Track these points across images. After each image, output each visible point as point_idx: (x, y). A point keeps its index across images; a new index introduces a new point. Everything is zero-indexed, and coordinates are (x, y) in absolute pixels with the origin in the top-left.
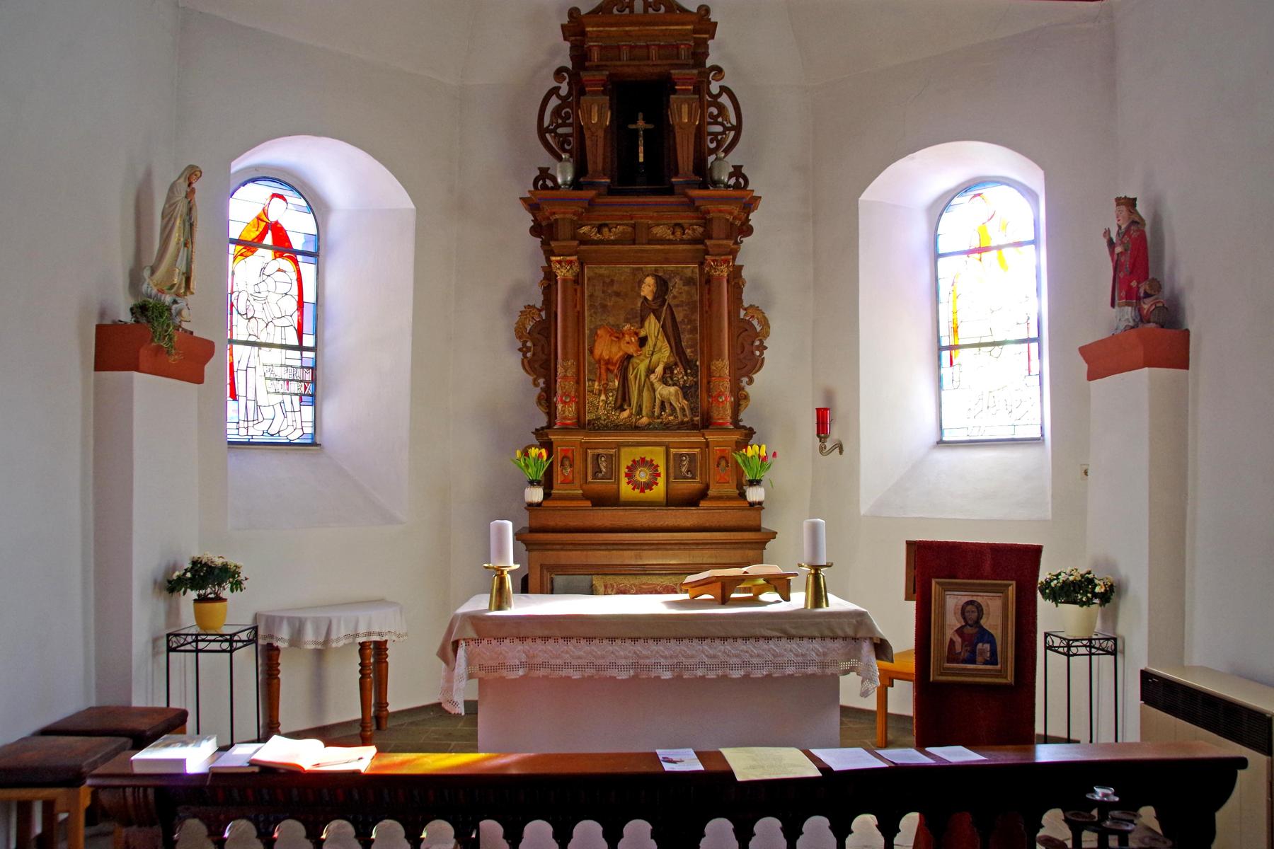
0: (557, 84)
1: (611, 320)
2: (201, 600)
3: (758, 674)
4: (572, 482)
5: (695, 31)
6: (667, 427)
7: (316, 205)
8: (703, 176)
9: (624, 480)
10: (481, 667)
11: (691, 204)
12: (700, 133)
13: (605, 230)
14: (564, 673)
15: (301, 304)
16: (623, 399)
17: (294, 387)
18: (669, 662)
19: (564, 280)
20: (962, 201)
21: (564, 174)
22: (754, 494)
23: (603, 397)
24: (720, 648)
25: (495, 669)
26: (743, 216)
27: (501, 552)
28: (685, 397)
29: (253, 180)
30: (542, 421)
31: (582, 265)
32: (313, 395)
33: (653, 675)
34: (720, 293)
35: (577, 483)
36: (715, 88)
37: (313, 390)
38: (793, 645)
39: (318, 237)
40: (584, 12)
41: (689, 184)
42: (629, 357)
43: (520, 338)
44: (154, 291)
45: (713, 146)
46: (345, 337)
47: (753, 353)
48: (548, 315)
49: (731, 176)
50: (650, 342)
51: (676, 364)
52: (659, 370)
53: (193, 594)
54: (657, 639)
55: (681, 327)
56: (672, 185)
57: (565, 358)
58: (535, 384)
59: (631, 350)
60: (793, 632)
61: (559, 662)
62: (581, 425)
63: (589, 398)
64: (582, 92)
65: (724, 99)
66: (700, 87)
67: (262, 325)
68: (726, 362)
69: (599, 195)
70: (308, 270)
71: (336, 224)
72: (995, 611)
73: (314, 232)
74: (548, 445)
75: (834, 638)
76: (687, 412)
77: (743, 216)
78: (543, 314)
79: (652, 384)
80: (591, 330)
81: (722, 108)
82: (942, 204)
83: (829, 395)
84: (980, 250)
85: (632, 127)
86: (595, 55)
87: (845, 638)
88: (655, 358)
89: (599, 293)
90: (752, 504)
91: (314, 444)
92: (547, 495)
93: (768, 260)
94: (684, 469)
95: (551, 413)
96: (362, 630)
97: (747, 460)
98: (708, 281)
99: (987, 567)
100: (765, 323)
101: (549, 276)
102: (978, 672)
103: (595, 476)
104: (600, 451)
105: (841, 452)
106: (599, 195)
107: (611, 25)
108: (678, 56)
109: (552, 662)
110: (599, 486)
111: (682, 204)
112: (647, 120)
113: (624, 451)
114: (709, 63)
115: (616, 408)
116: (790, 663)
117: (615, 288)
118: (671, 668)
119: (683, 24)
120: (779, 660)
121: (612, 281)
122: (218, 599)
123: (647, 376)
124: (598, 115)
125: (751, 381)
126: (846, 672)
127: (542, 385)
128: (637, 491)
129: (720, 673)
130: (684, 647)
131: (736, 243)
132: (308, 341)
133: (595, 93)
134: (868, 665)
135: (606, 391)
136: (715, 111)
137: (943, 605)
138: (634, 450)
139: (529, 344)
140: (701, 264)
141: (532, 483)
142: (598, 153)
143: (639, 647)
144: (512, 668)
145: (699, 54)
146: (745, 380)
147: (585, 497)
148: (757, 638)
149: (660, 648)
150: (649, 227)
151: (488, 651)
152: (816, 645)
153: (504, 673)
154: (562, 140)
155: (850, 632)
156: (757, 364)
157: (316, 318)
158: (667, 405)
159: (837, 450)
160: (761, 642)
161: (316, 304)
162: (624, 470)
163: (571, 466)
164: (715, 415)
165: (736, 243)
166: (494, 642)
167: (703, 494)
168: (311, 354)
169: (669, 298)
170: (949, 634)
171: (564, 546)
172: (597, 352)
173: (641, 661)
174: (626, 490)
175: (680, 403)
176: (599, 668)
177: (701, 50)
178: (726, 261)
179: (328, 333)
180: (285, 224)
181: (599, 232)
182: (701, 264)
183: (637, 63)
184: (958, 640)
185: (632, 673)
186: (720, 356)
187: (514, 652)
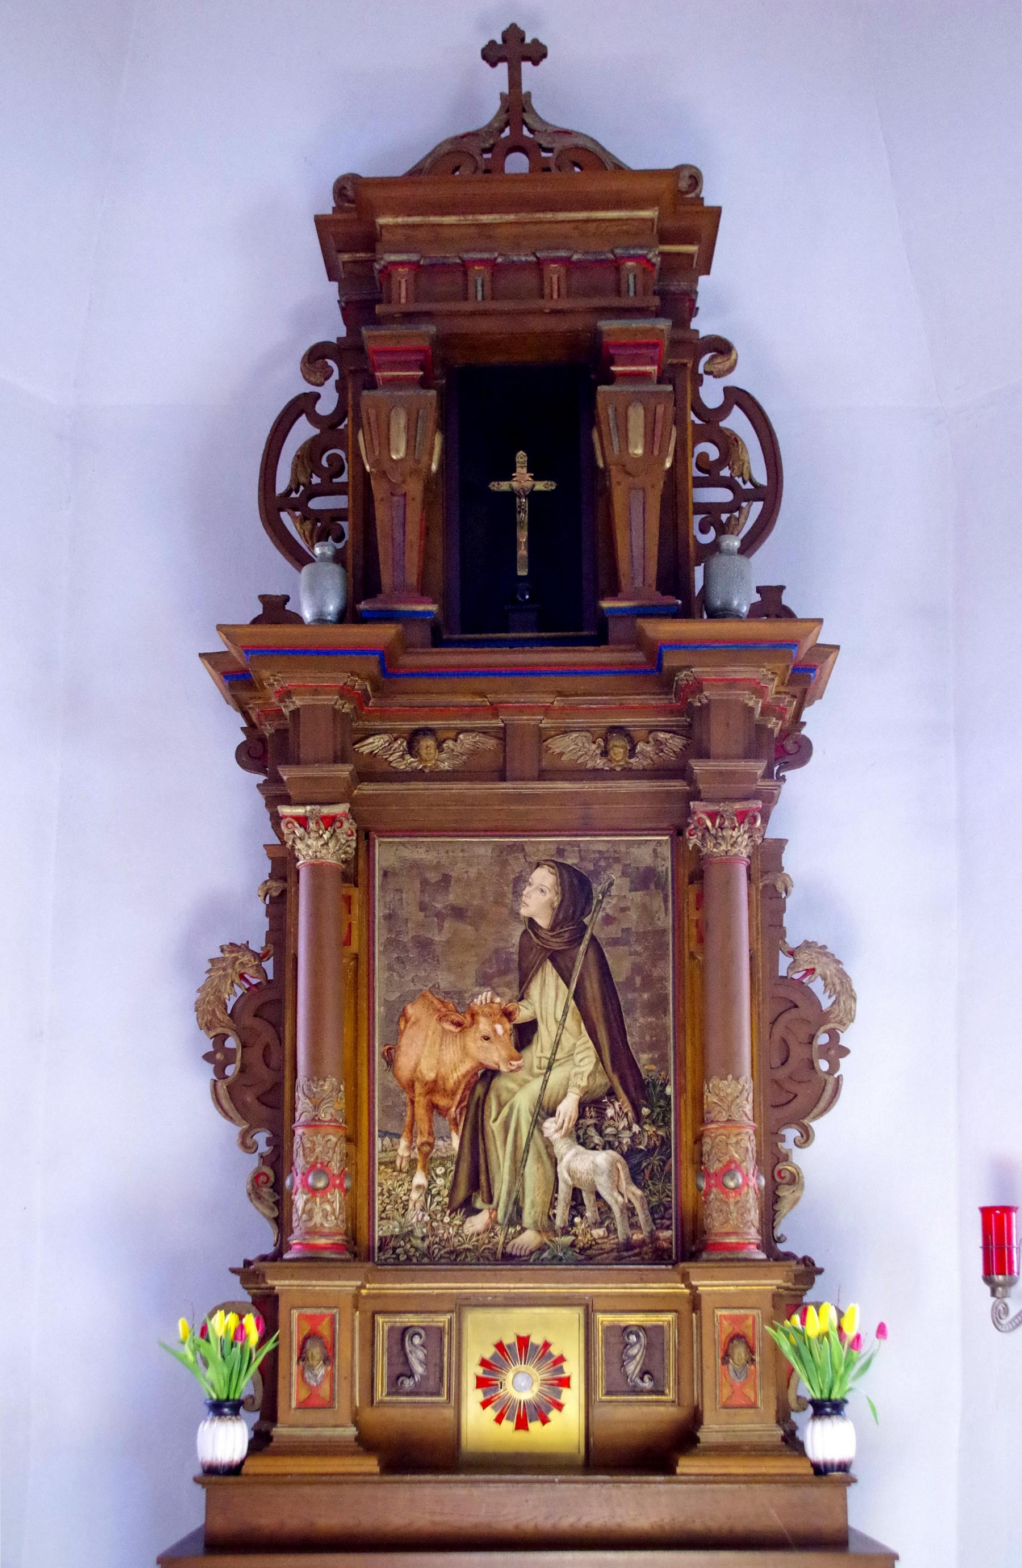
0: (309, 388)
1: (444, 980)
5: (664, 238)
6: (586, 1256)
8: (676, 586)
9: (473, 1397)
13: (427, 744)
16: (474, 1182)
19: (317, 869)
21: (316, 595)
23: (420, 1178)
28: (636, 1176)
31: (365, 836)
36: (711, 394)
42: (488, 1075)
43: (208, 1026)
47: (812, 1066)
48: (279, 967)
50: (545, 1036)
51: (611, 1093)
52: (568, 1108)
57: (316, 1073)
58: (246, 1144)
59: (495, 1055)
62: (358, 1249)
65: (737, 422)
69: (407, 645)
76: (642, 1217)
78: (268, 965)
79: (549, 1145)
81: (729, 444)
85: (504, 486)
88: (556, 1076)
89: (410, 910)
90: (820, 1470)
92: (260, 1442)
98: (698, 876)
101: (283, 865)
103: (395, 1386)
106: (407, 645)
110: (406, 1414)
112: (537, 471)
115: (453, 1209)
121: (446, 879)
123: (537, 1123)
124: (406, 441)
125: (806, 1137)
135: (429, 1161)
136: (713, 452)
138: (498, 1315)
142: (406, 538)
145: (680, 306)
146: (791, 1133)
150: (542, 736)
158: (588, 1199)
162: (472, 1370)
163: (328, 1359)
164: (716, 1224)
169: (594, 923)
172: (405, 1063)
175: (621, 1193)
181: (412, 749)
186: (729, 1068)
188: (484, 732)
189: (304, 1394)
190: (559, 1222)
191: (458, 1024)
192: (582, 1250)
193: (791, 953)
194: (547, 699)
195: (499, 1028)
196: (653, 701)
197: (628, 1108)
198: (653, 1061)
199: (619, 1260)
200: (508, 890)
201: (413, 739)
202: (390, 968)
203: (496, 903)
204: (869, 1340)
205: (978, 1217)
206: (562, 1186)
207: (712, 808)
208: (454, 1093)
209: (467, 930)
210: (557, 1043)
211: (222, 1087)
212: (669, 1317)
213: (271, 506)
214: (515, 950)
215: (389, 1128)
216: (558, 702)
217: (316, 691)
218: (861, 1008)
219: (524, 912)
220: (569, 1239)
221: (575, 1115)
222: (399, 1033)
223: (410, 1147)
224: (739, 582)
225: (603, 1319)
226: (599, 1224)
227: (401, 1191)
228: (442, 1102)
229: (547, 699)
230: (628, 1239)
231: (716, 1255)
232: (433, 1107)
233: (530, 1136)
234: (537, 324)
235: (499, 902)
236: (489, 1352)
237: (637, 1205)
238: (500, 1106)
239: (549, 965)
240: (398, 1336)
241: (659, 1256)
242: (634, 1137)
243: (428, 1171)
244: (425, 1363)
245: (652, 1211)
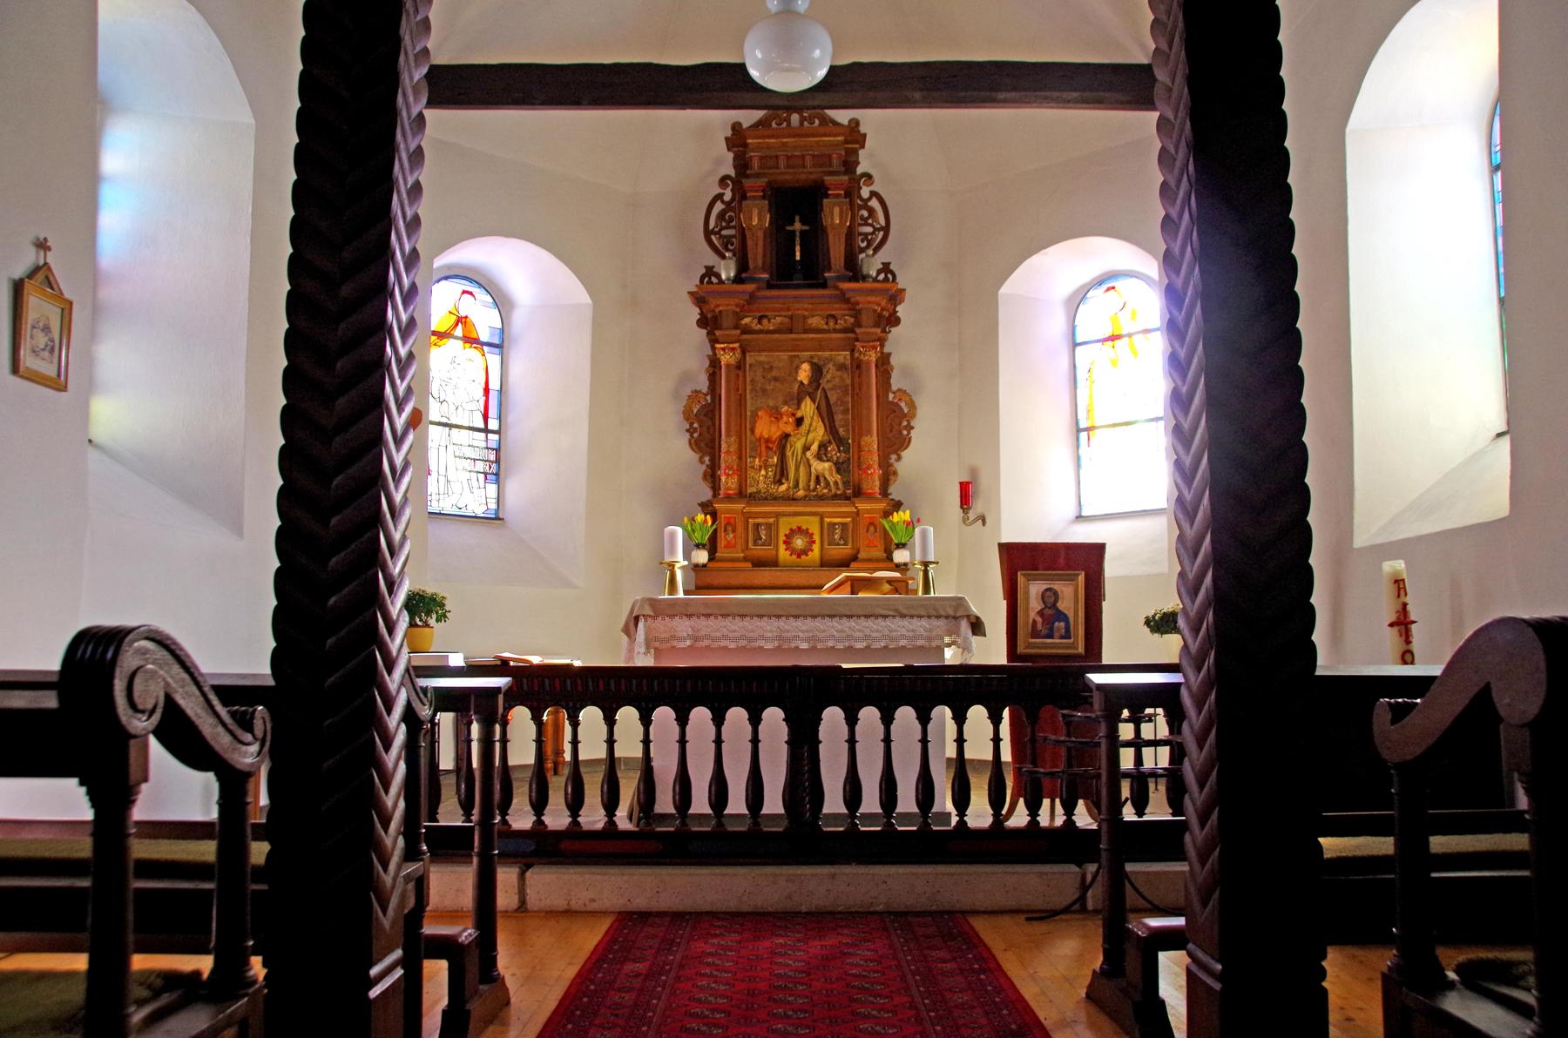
1: (771, 403)
3: (876, 645)
5: (846, 142)
6: (821, 498)
7: (502, 302)
8: (854, 271)
10: (657, 639)
11: (843, 298)
12: (851, 235)
13: (765, 321)
15: (487, 390)
16: (782, 474)
17: (480, 466)
19: (728, 366)
20: (1096, 294)
21: (727, 270)
22: (900, 556)
24: (846, 624)
26: (891, 308)
27: (673, 551)
28: (838, 471)
29: (446, 278)
30: (706, 493)
31: (744, 353)
32: (497, 474)
33: (793, 645)
34: (869, 377)
35: (739, 547)
36: (865, 192)
37: (496, 472)
38: (905, 622)
39: (502, 330)
40: (745, 126)
41: (841, 278)
42: (787, 436)
43: (687, 419)
45: (864, 245)
46: (525, 422)
48: (713, 399)
49: (879, 272)
50: (807, 422)
52: (815, 447)
54: (796, 617)
55: (834, 409)
56: (826, 280)
57: (728, 435)
58: (702, 462)
59: (789, 429)
62: (741, 494)
63: (751, 473)
64: (744, 197)
65: (874, 203)
66: (851, 192)
67: (453, 408)
68: (875, 438)
69: (758, 289)
71: (519, 318)
72: (1070, 595)
74: (714, 516)
75: (938, 617)
77: (891, 308)
81: (871, 211)
82: (1077, 299)
83: (974, 472)
84: (1113, 338)
86: (756, 164)
87: (947, 617)
88: (810, 437)
89: (759, 378)
93: (914, 347)
95: (715, 488)
97: (893, 525)
98: (858, 367)
99: (1061, 561)
100: (912, 405)
101: (714, 363)
102: (1054, 645)
103: (755, 543)
106: (758, 289)
107: (772, 137)
110: (760, 551)
111: (831, 296)
112: (803, 222)
113: (782, 520)
114: (860, 170)
117: (774, 374)
118: (808, 640)
123: (804, 453)
124: (758, 217)
125: (899, 458)
126: (949, 645)
130: (818, 623)
131: (884, 331)
132: (493, 424)
133: (755, 198)
134: (966, 639)
136: (865, 214)
137: (1027, 592)
138: (791, 519)
140: (853, 351)
141: (698, 546)
142: (758, 252)
143: (782, 623)
145: (850, 165)
146: (894, 457)
147: (745, 559)
148: (877, 617)
149: (799, 623)
150: (805, 318)
151: (662, 626)
152: (924, 622)
154: (727, 242)
155: (951, 612)
156: (904, 443)
157: (500, 404)
161: (501, 391)
162: (782, 538)
163: (734, 531)
164: (864, 486)
165: (884, 331)
167: (855, 558)
168: (496, 437)
169: (823, 382)
170: (1033, 615)
172: (758, 432)
176: (750, 640)
177: (852, 159)
178: (874, 347)
179: (512, 417)
180: (473, 318)
181: (760, 322)
182: (853, 351)
184: (1039, 620)
186: (869, 432)
201: (760, 319)
213: (708, 233)
224: (871, 265)
234: (803, 177)
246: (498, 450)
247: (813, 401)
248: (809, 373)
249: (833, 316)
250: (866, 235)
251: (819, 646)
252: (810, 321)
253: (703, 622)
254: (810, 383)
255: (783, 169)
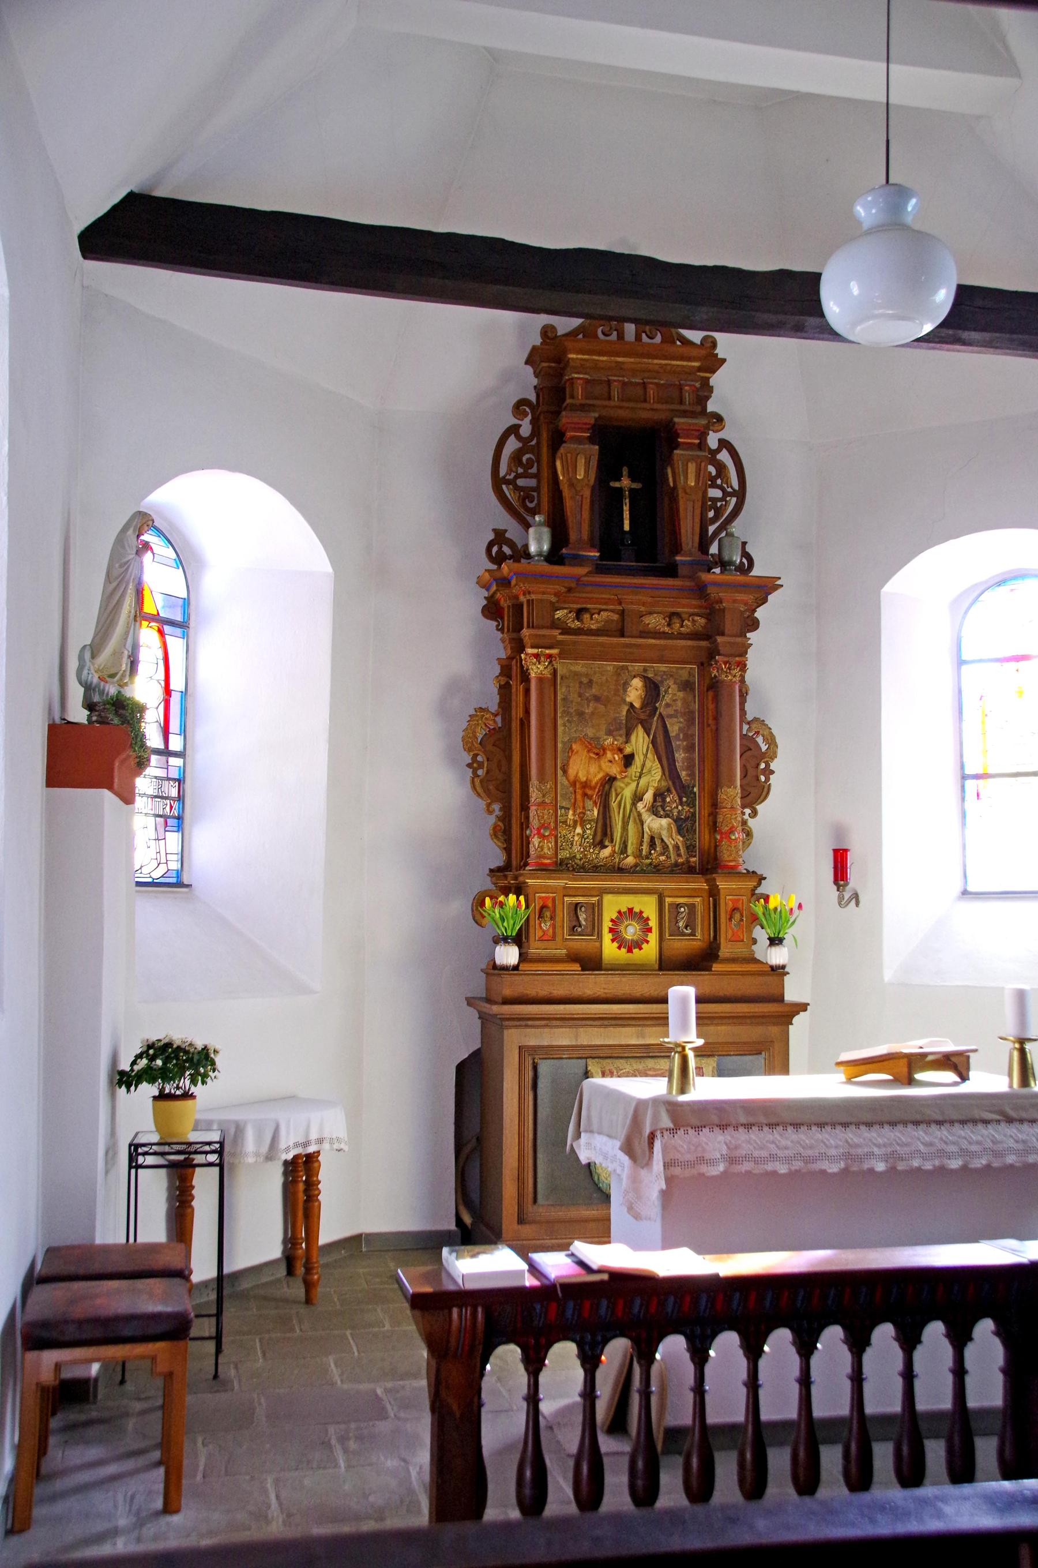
0: (516, 422)
1: (590, 732)
2: (162, 1097)
4: (554, 938)
6: (657, 870)
9: (607, 937)
11: (701, 590)
13: (586, 616)
14: (770, 1167)
15: (168, 691)
16: (604, 833)
18: (883, 1151)
19: (540, 680)
21: (538, 542)
23: (579, 830)
25: (690, 1164)
28: (680, 831)
32: (180, 818)
38: (1012, 1130)
42: (612, 779)
43: (469, 750)
44: (96, 680)
47: (758, 779)
50: (638, 761)
51: (669, 790)
52: (649, 797)
53: (153, 1090)
54: (869, 1125)
55: (675, 743)
59: (615, 770)
60: (1013, 1114)
61: (764, 1154)
63: (563, 831)
65: (724, 456)
70: (176, 645)
73: (184, 594)
76: (682, 851)
78: (499, 719)
79: (639, 815)
80: (564, 743)
81: (721, 468)
83: (839, 831)
85: (617, 485)
88: (643, 782)
90: (774, 969)
91: (180, 884)
92: (523, 957)
94: (681, 924)
96: (314, 1136)
100: (771, 741)
104: (580, 899)
105: (857, 904)
108: (681, 402)
109: (756, 1154)
110: (581, 944)
111: (681, 589)
112: (633, 478)
113: (608, 899)
115: (594, 845)
116: (1011, 1150)
117: (594, 691)
118: (885, 1158)
119: (689, 359)
120: (999, 1147)
121: (591, 681)
122: (187, 1096)
123: (634, 804)
124: (579, 468)
125: (754, 814)
127: (497, 812)
128: (624, 950)
129: (937, 1163)
132: (176, 743)
133: (579, 440)
135: (583, 822)
139: (479, 758)
142: (581, 519)
143: (850, 1135)
144: (712, 1162)
146: (748, 811)
151: (684, 1142)
153: (704, 1169)
154: (526, 495)
158: (658, 842)
159: (853, 902)
160: (980, 1126)
162: (607, 924)
163: (552, 918)
166: (691, 1131)
169: (661, 707)
171: (549, 1021)
172: (572, 772)
173: (853, 1151)
174: (610, 950)
175: (673, 839)
176: (808, 1160)
179: (200, 734)
181: (578, 617)
183: (631, 405)
185: (842, 1165)
186: (731, 783)
187: (715, 1143)
188: (612, 611)
189: (541, 934)
190: (644, 853)
191: (597, 754)
192: (655, 866)
193: (749, 723)
194: (644, 599)
195: (616, 757)
196: (694, 602)
197: (676, 798)
198: (688, 775)
199: (672, 872)
200: (621, 688)
201: (579, 613)
202: (564, 725)
203: (615, 694)
204: (795, 910)
205: (831, 853)
206: (646, 835)
207: (726, 659)
208: (595, 788)
209: (601, 708)
210: (643, 765)
211: (477, 781)
212: (698, 899)
214: (624, 718)
215: (564, 804)
216: (650, 600)
217: (544, 593)
218: (780, 751)
219: (628, 700)
220: (649, 861)
221: (652, 800)
222: (569, 757)
223: (574, 815)
225: (668, 900)
226: (662, 854)
227: (570, 836)
228: (589, 792)
229: (644, 599)
230: (676, 862)
231: (725, 871)
232: (585, 795)
233: (631, 811)
234: (644, 415)
235: (616, 693)
236: (614, 916)
237: (680, 844)
238: (617, 795)
239: (640, 727)
240: (573, 907)
241: (691, 870)
242: (679, 812)
243: (583, 827)
244: (586, 920)
245: (687, 848)
246: (180, 782)
247: (647, 732)
248: (641, 692)
249: (678, 615)
250: (714, 500)
251: (901, 1166)
252: (647, 620)
253: (742, 1135)
254: (644, 706)
255: (615, 402)
